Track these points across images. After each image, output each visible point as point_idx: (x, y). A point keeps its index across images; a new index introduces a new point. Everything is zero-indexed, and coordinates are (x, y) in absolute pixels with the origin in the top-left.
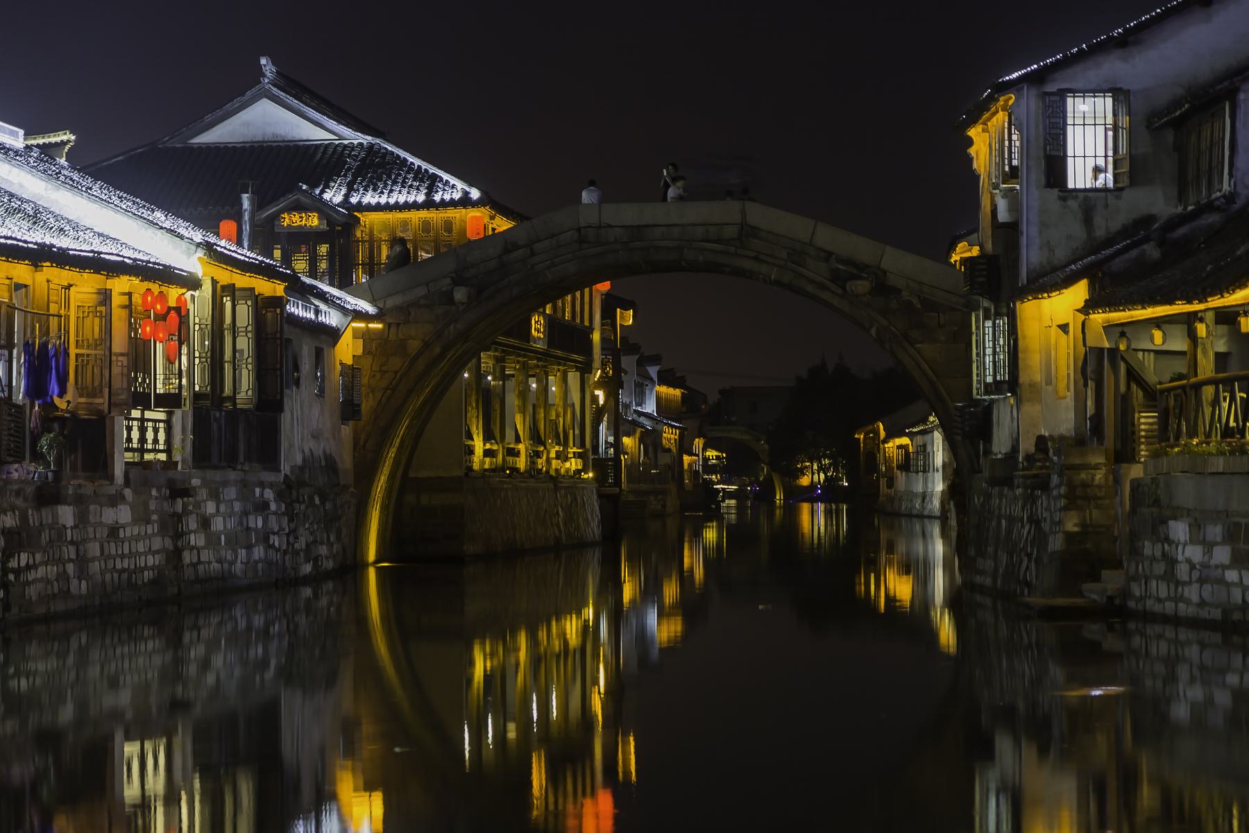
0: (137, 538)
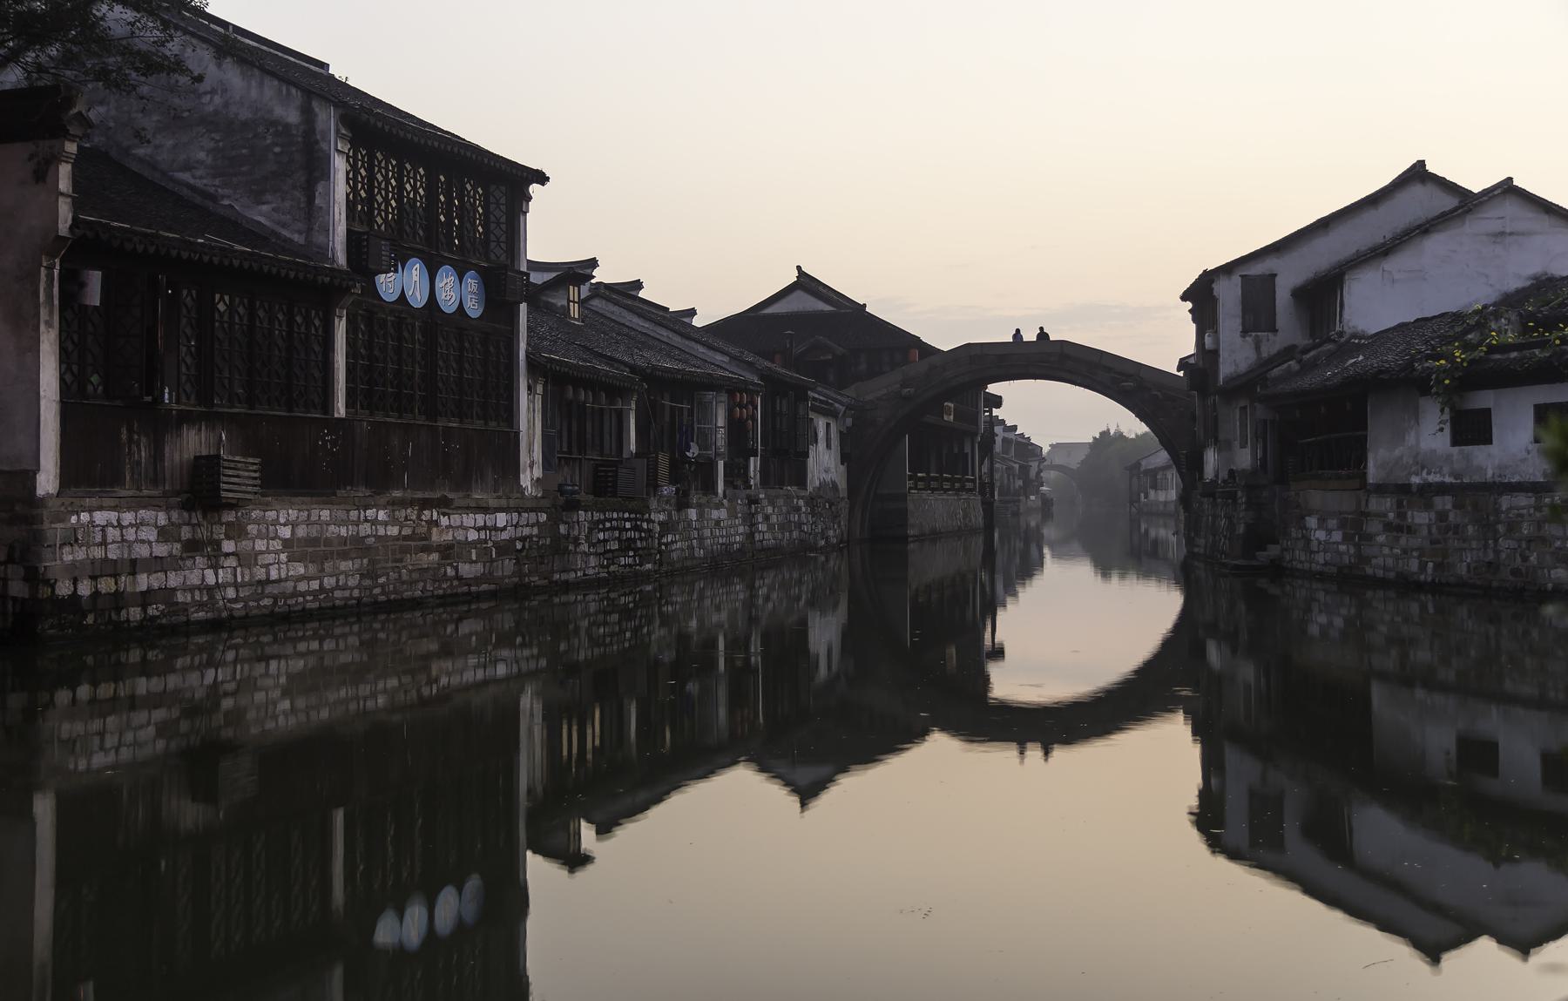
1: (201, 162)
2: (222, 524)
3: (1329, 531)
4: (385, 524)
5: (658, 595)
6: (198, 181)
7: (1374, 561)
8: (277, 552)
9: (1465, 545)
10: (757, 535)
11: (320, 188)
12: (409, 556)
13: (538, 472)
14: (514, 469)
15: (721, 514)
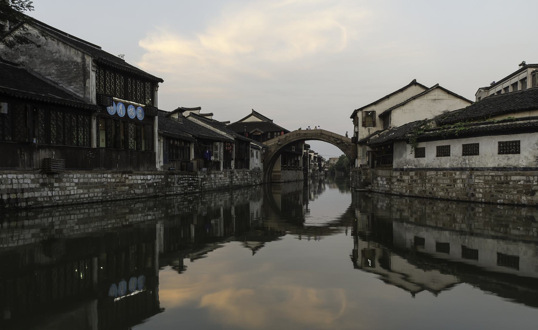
1: (53, 73)
2: (54, 178)
3: (383, 181)
4: (111, 178)
5: (201, 197)
6: (53, 79)
7: (394, 190)
8: (73, 186)
9: (418, 185)
11: (87, 81)
12: (118, 187)
13: (162, 164)
14: (154, 163)
15: (222, 176)
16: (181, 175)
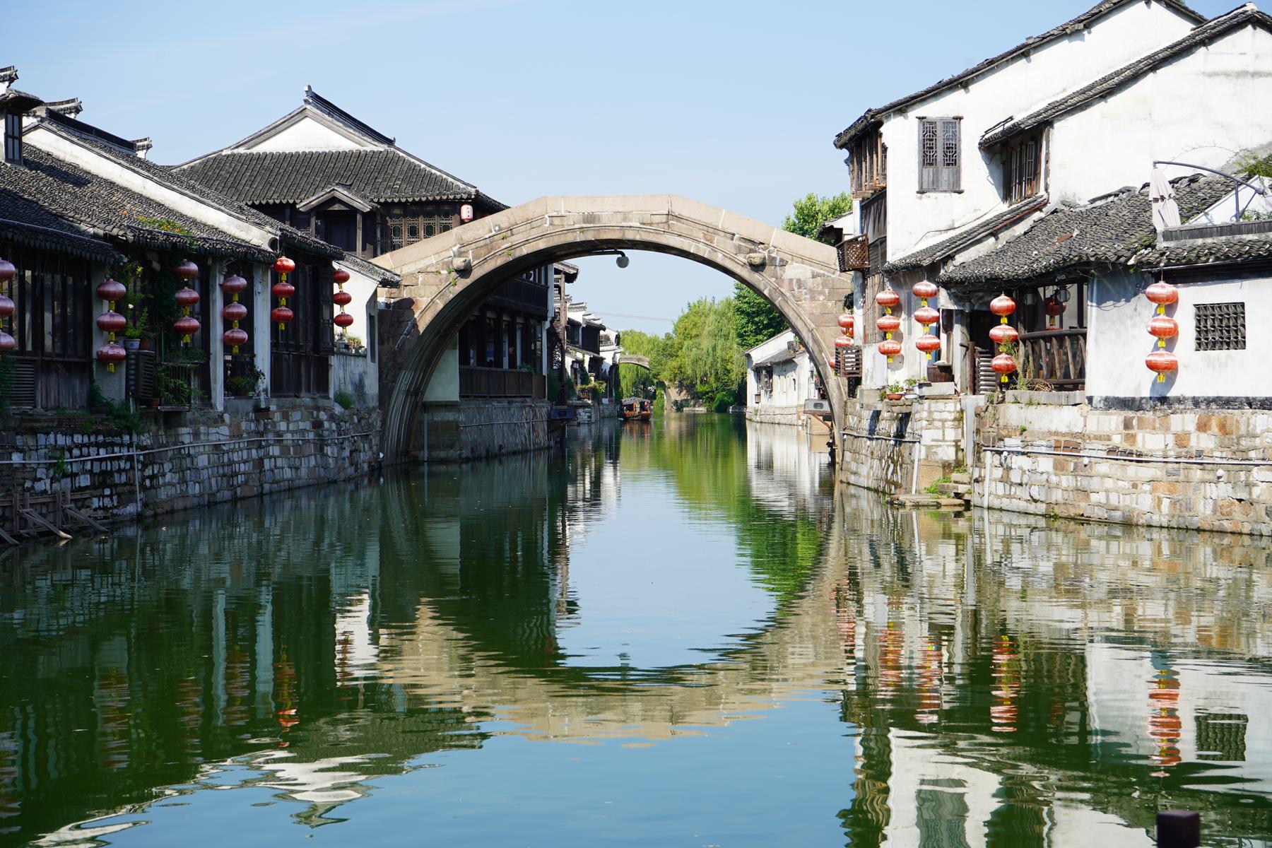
0: (233, 451)
10: (266, 462)
16: (65, 434)
